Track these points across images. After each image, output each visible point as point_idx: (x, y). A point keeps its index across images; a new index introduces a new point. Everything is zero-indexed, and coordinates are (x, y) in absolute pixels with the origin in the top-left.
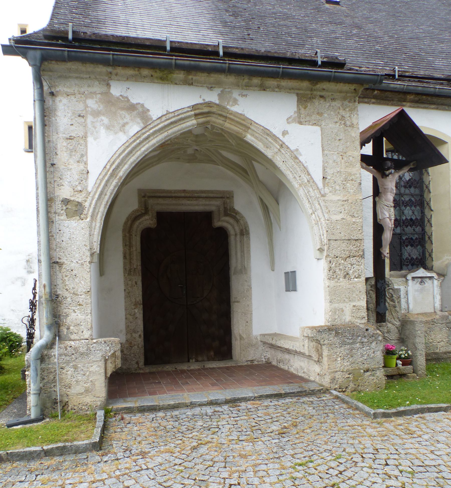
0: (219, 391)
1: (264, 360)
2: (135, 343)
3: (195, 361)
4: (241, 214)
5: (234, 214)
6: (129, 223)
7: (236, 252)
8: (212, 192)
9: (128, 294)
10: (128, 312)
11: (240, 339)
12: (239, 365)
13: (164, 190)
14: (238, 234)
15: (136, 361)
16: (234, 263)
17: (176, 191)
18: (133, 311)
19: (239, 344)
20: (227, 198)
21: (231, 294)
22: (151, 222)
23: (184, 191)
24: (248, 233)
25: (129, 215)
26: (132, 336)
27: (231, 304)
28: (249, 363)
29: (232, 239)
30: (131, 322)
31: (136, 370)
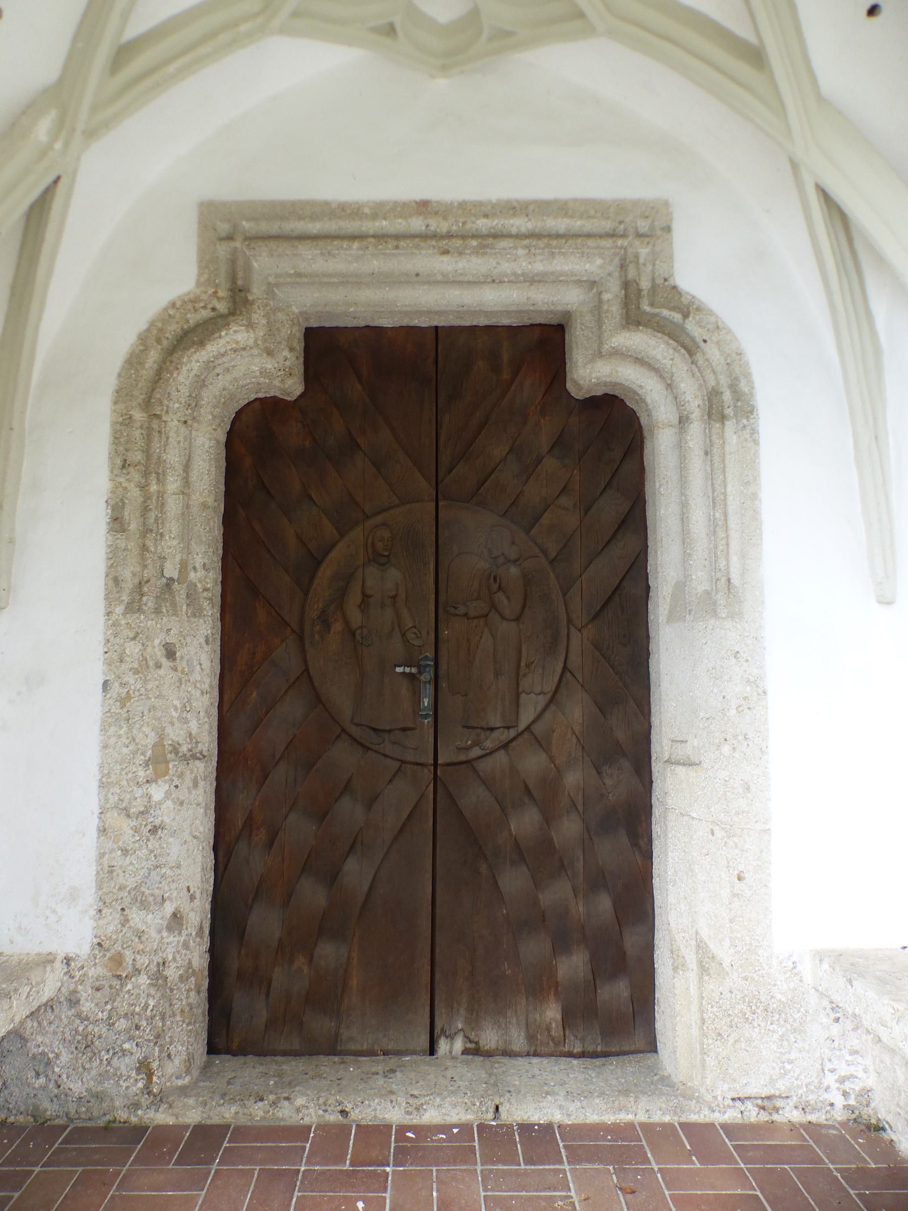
0: (660, 589)
1: (839, 1101)
2: (143, 961)
3: (466, 1052)
4: (711, 313)
5: (677, 317)
6: (153, 357)
7: (684, 505)
8: (562, 208)
9: (120, 702)
10: (113, 799)
11: (703, 969)
12: (693, 1118)
13: (327, 203)
14: (696, 414)
15: (138, 1055)
16: (671, 564)
17: (380, 210)
18: (139, 792)
19: (694, 991)
20: (639, 235)
21: (655, 720)
22: (270, 365)
23: (423, 207)
24: (745, 408)
25: (152, 324)
26: (125, 921)
27: (656, 767)
28: (753, 1115)
29: (662, 450)
30: (125, 852)
31: (136, 1106)
